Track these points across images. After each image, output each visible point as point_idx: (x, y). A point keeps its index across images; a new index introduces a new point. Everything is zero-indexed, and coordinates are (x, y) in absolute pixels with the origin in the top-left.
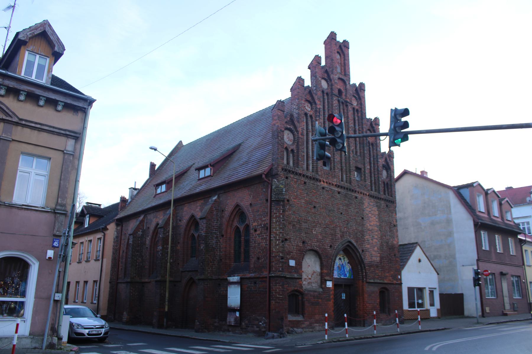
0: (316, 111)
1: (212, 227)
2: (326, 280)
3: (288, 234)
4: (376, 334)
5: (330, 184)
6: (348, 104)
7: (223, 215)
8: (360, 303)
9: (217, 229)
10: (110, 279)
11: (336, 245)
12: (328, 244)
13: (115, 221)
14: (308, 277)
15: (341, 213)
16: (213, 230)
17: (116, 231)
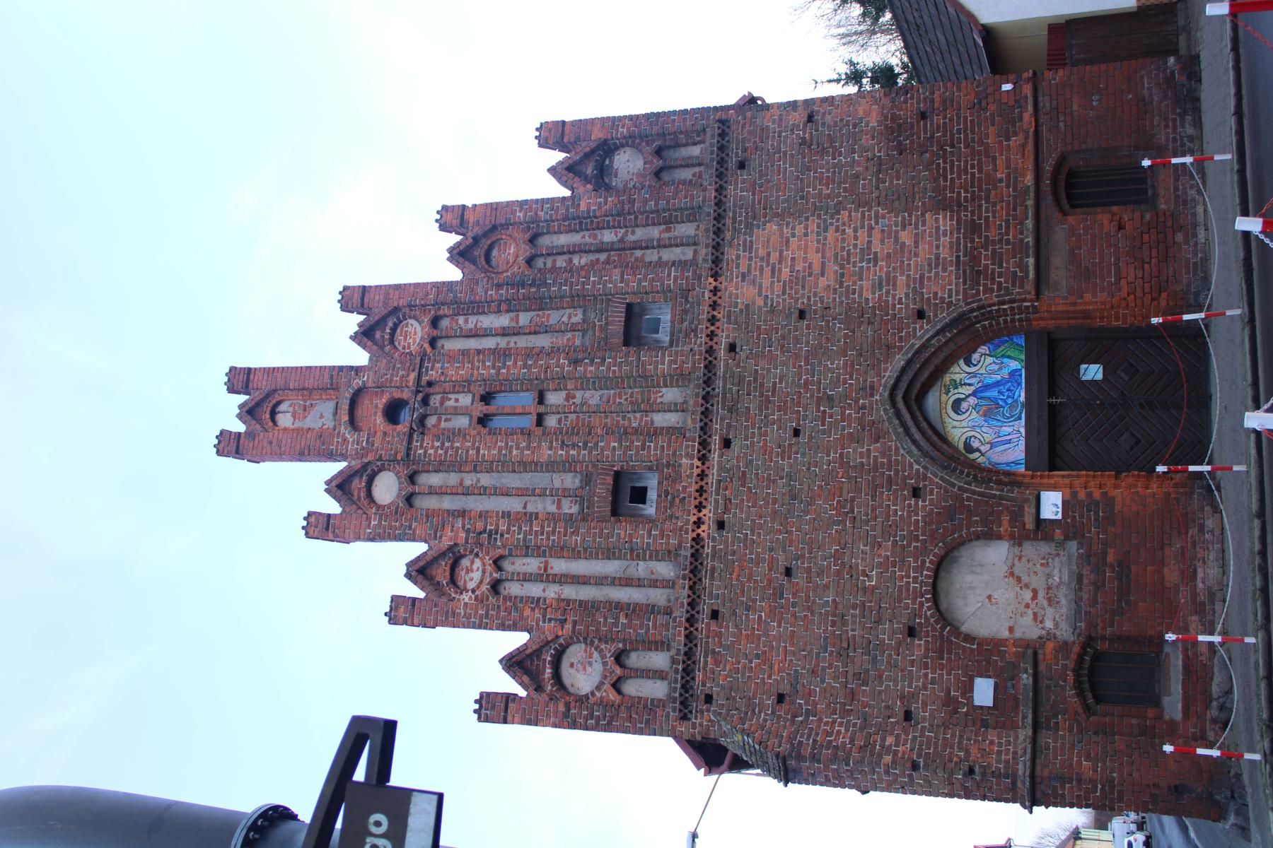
2: (1039, 521)
3: (887, 707)
4: (1249, 465)
6: (423, 383)
8: (1117, 319)
11: (911, 465)
12: (909, 505)
14: (1027, 606)
15: (796, 433)
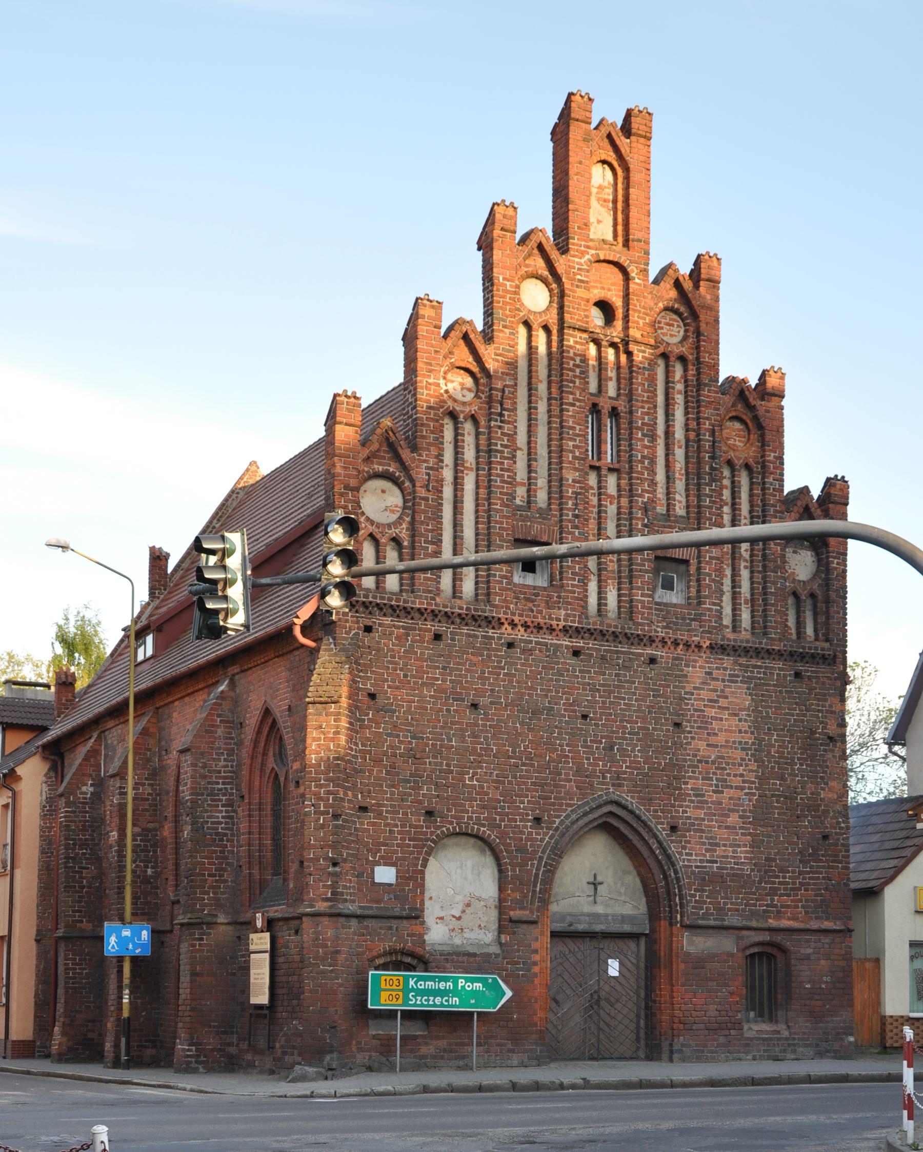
0: (490, 400)
1: (214, 775)
5: (539, 628)
7: (243, 736)
9: (231, 778)
10: (38, 930)
13: (40, 749)
15: (585, 717)
16: (218, 783)
17: (46, 782)
